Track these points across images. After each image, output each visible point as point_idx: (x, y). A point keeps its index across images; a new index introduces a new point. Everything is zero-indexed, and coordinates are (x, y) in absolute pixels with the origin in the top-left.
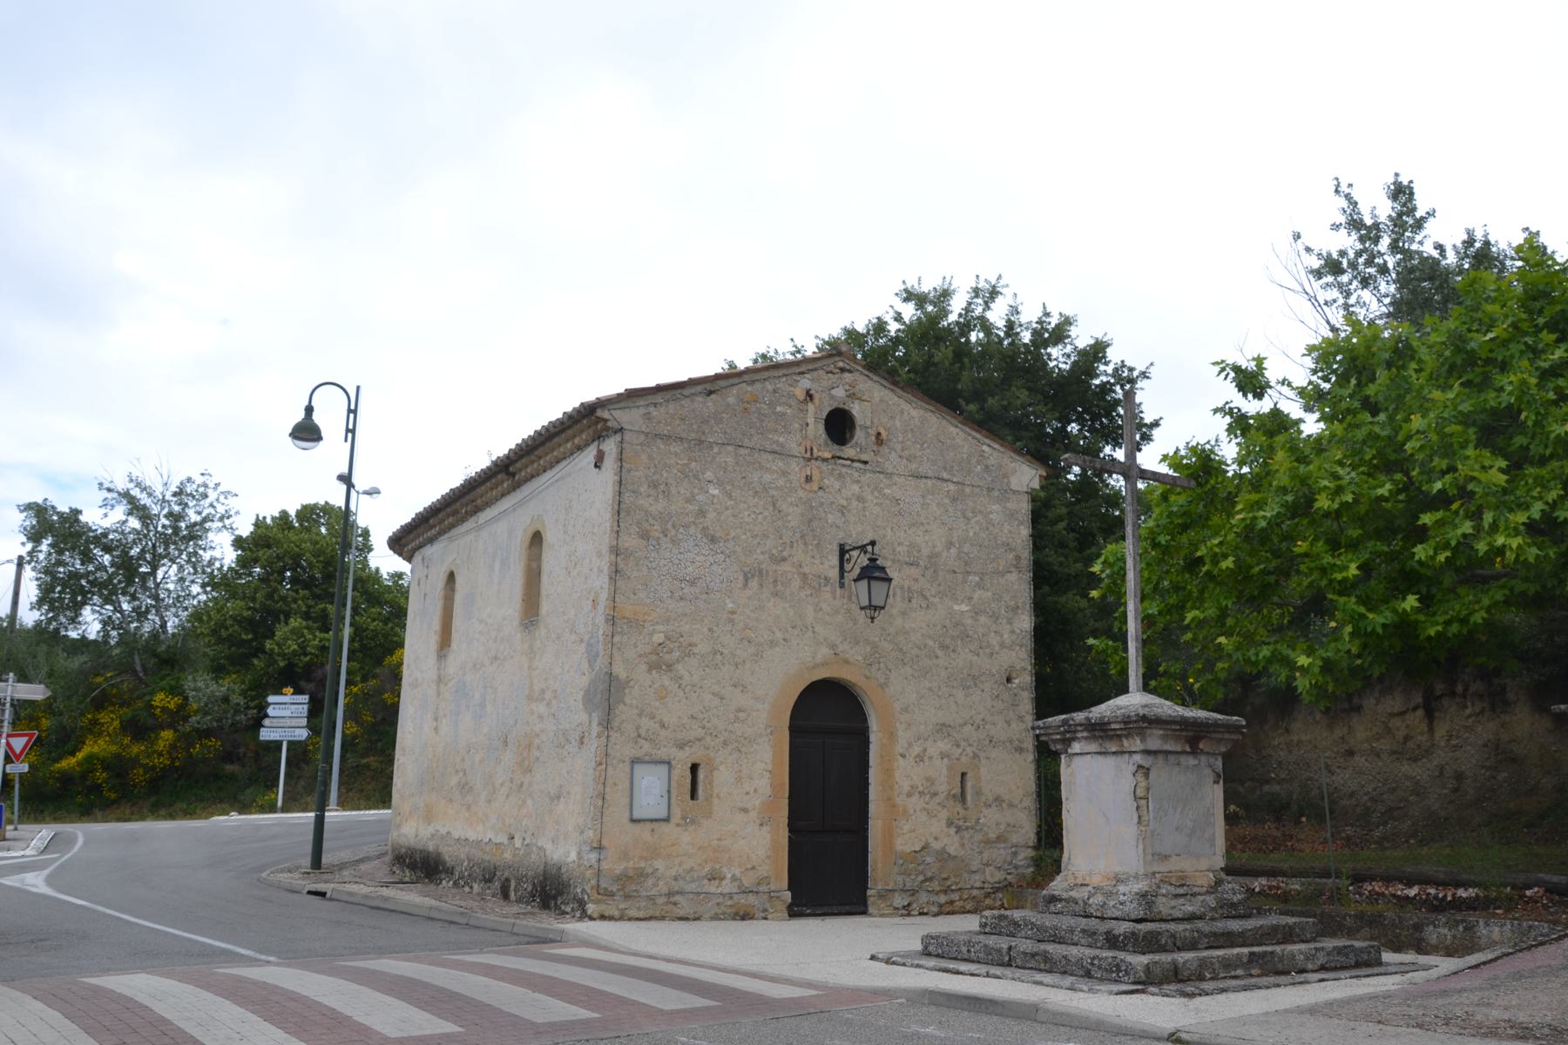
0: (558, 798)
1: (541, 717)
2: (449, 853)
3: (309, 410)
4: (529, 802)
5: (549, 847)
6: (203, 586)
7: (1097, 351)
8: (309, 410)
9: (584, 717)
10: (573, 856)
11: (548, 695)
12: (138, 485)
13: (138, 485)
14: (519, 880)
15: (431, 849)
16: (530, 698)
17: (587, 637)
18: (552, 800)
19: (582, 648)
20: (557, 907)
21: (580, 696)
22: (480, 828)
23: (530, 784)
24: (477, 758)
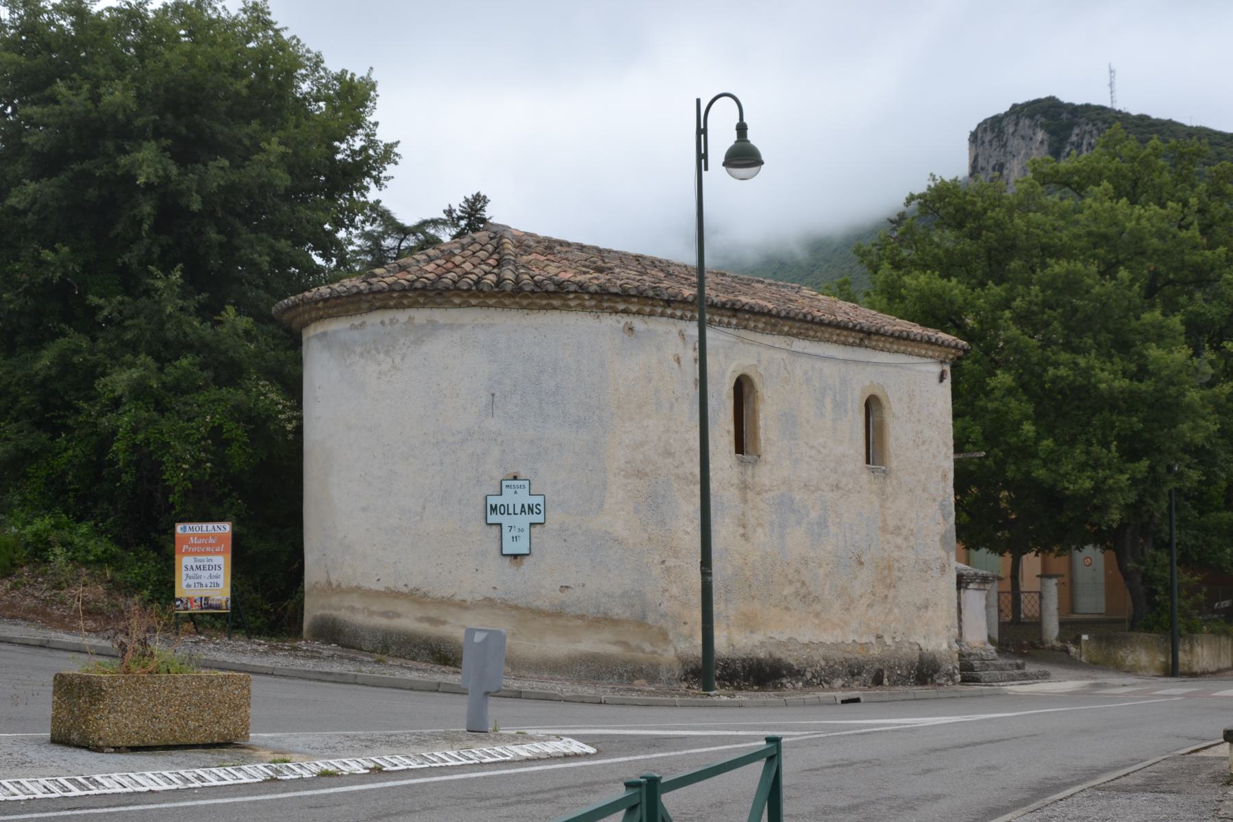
0: (926, 607)
1: (899, 547)
2: (791, 657)
3: (742, 129)
4: (896, 610)
5: (922, 642)
6: (22, 511)
7: (467, 200)
8: (742, 129)
9: (943, 553)
10: (945, 646)
11: (904, 532)
12: (492, 325)
13: (492, 325)
14: (891, 668)
15: (762, 656)
16: (884, 529)
17: (940, 499)
18: (919, 609)
19: (936, 506)
20: (933, 682)
21: (937, 538)
22: (838, 632)
23: (895, 597)
24: (821, 572)
